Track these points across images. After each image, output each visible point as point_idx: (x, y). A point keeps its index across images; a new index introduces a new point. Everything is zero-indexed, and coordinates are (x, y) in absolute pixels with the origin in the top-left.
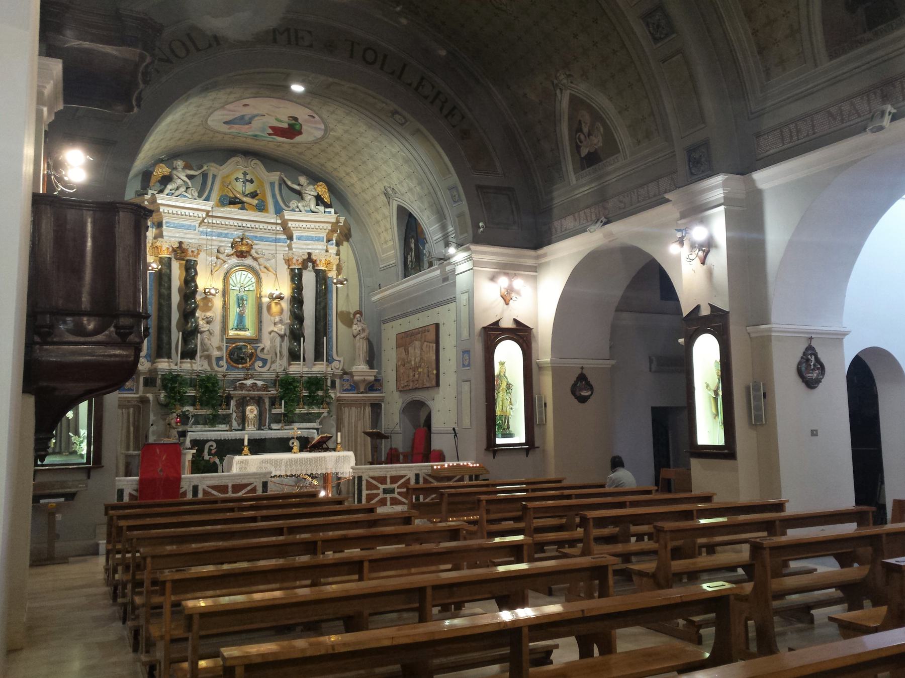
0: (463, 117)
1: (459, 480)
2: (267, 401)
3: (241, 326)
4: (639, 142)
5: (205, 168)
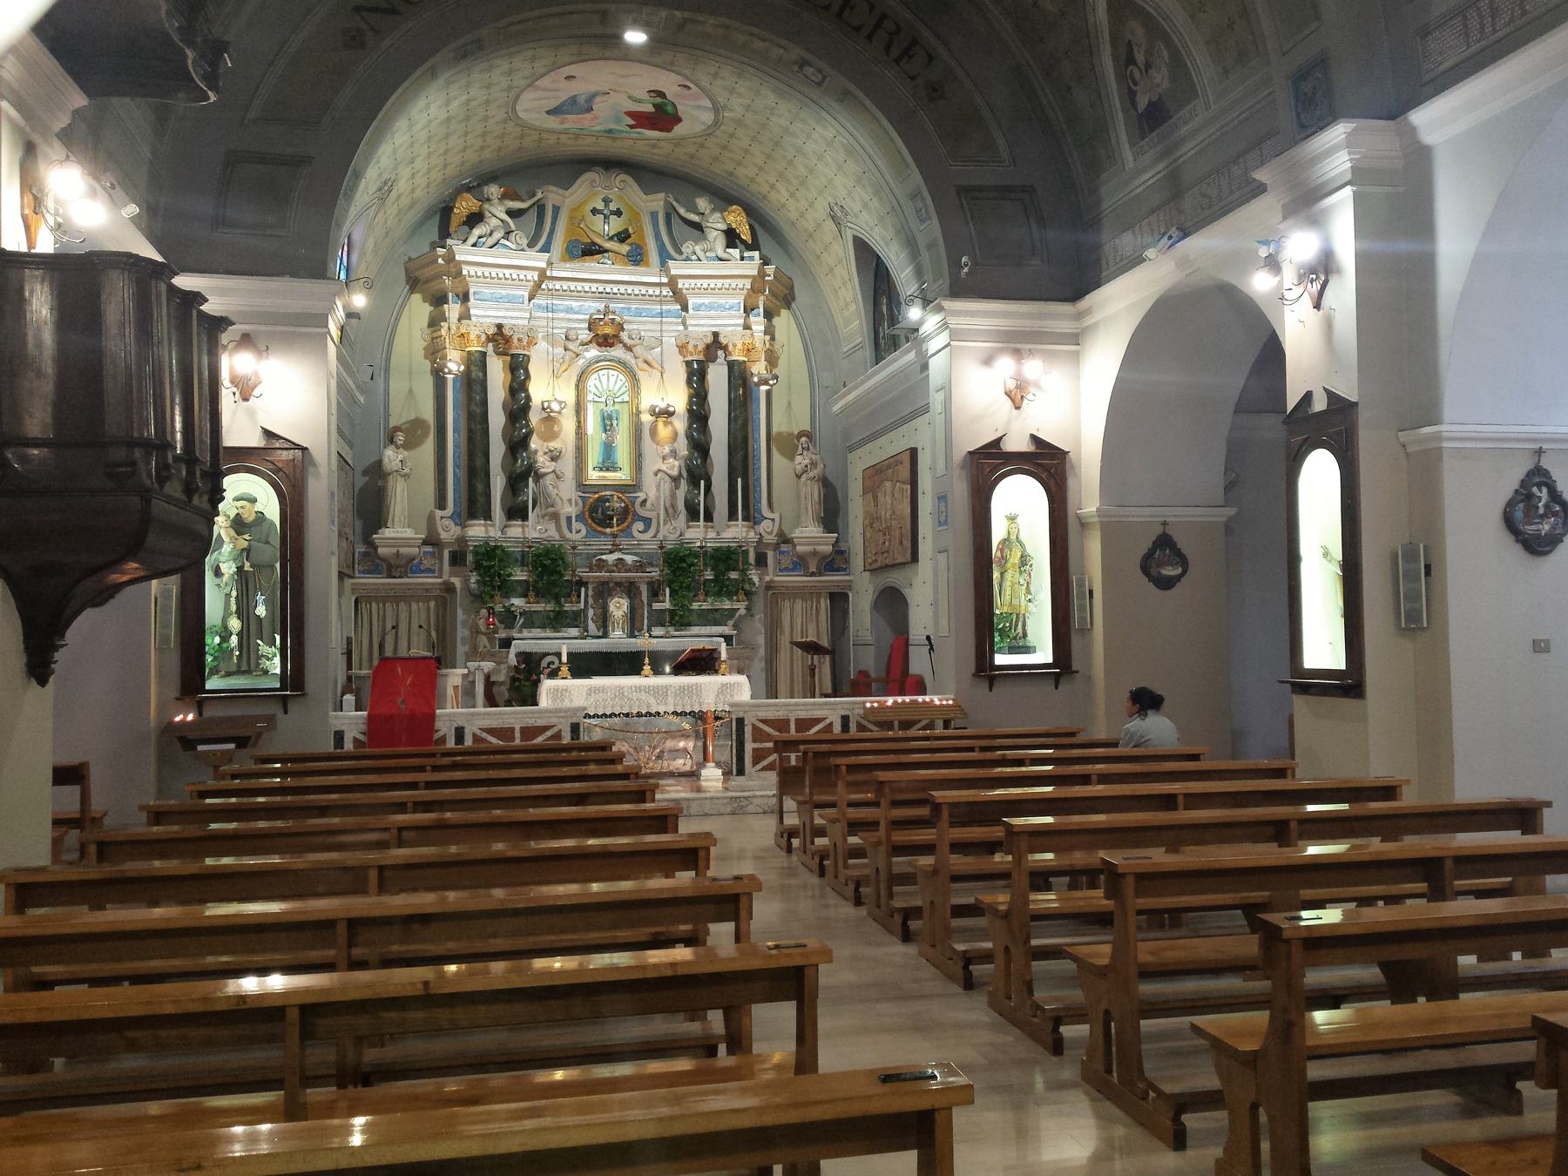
0: (931, 58)
1: (924, 728)
2: (644, 590)
3: (608, 464)
4: (1226, 72)
5: (539, 195)
